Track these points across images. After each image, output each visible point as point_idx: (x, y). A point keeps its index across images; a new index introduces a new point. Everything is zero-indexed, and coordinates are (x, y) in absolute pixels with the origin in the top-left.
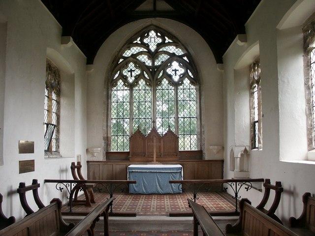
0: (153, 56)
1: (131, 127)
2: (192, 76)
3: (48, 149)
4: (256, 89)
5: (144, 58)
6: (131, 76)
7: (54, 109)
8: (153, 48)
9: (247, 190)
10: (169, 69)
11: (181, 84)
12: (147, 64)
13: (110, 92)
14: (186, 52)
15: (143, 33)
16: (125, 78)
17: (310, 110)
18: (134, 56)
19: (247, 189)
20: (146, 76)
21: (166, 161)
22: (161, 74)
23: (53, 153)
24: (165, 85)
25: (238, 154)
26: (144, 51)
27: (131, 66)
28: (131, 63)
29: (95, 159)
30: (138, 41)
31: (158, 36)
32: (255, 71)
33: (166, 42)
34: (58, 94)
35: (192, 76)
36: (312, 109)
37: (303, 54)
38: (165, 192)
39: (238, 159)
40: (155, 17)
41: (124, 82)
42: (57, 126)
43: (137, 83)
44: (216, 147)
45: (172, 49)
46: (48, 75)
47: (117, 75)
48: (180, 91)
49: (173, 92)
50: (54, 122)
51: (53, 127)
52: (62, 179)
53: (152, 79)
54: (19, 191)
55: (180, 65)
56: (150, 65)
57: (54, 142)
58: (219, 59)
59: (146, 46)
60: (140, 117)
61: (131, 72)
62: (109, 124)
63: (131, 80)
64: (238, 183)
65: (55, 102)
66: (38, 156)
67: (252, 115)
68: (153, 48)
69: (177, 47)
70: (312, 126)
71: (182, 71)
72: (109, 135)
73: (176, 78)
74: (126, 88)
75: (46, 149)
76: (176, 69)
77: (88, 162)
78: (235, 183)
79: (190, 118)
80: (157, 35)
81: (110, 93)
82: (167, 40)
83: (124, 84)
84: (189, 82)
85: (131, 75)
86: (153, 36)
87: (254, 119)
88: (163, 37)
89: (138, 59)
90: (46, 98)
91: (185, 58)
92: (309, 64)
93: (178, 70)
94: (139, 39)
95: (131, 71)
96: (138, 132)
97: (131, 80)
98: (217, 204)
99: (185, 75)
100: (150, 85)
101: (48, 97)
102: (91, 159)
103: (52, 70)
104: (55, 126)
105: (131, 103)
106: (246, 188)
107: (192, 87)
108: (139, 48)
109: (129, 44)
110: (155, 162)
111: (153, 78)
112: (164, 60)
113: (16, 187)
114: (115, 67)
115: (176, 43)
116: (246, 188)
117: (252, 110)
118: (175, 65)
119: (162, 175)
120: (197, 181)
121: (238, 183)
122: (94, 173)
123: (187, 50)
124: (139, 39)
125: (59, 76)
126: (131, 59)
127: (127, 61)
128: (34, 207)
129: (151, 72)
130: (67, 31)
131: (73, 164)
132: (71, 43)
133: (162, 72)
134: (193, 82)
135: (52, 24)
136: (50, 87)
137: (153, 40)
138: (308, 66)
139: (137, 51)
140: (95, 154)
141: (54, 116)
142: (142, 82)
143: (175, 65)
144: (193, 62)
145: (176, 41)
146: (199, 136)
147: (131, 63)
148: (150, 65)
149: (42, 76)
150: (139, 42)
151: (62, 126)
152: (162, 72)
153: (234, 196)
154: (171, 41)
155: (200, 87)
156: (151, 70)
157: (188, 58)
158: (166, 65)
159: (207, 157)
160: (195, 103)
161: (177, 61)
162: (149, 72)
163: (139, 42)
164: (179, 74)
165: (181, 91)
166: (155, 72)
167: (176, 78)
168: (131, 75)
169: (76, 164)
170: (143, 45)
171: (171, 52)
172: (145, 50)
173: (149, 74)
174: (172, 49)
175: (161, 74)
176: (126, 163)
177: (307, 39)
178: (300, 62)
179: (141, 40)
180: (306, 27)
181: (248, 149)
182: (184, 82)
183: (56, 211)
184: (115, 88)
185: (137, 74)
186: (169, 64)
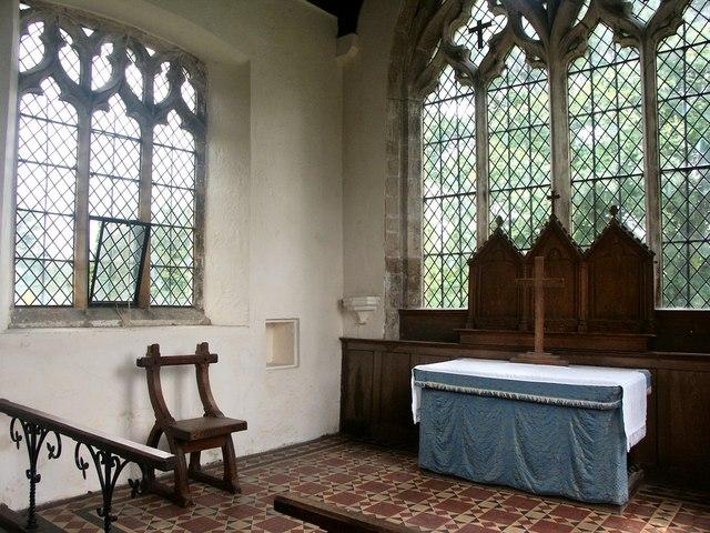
13: (412, 111)
16: (457, 56)
20: (530, 31)
21: (607, 352)
24: (602, 48)
29: (362, 333)
38: (545, 486)
49: (632, 72)
53: (545, 40)
62: (410, 218)
63: (477, 58)
74: (464, 90)
95: (480, 27)
99: (513, 34)
100: (542, 64)
110: (538, 353)
119: (540, 412)
122: (359, 377)
140: (364, 318)
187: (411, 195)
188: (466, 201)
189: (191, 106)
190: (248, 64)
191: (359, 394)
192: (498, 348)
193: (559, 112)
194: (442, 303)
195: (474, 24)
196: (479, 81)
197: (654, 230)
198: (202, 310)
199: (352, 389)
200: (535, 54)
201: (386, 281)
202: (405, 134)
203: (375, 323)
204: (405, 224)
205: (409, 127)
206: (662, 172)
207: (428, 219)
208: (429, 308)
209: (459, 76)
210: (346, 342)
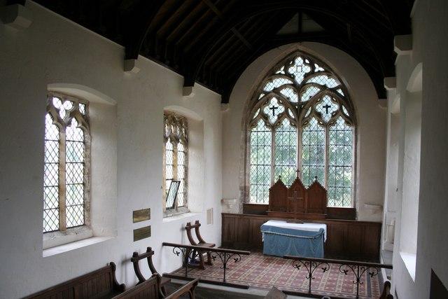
0: (300, 89)
2: (348, 114)
5: (289, 93)
8: (299, 79)
10: (319, 105)
14: (340, 84)
15: (288, 62)
16: (266, 118)
18: (276, 91)
21: (316, 219)
24: (314, 125)
27: (274, 101)
35: (348, 114)
44: (371, 206)
54: (132, 260)
59: (291, 77)
61: (274, 109)
68: (299, 79)
71: (335, 107)
72: (247, 185)
74: (267, 129)
76: (328, 106)
80: (304, 62)
82: (318, 68)
85: (274, 113)
91: (340, 91)
94: (282, 68)
95: (274, 108)
96: (280, 182)
97: (273, 120)
102: (226, 212)
109: (272, 75)
112: (313, 94)
113: (131, 255)
115: (328, 72)
118: (327, 100)
122: (229, 227)
123: (341, 81)
124: (282, 68)
126: (273, 94)
128: (147, 274)
133: (310, 108)
134: (350, 121)
137: (299, 69)
139: (281, 84)
140: (231, 206)
144: (349, 95)
150: (283, 73)
154: (322, 69)
158: (316, 99)
159: (360, 217)
161: (329, 95)
163: (283, 73)
164: (331, 112)
168: (274, 113)
171: (322, 84)
172: (290, 82)
179: (286, 70)
184: (255, 129)
185: (281, 112)
187: (248, 164)
190: (203, 121)
191: (229, 233)
192: (278, 217)
193: (300, 144)
195: (272, 107)
196: (327, 125)
197: (327, 185)
199: (226, 231)
200: (294, 123)
201: (239, 194)
202: (246, 142)
203: (235, 208)
204: (245, 174)
205: (247, 140)
209: (266, 125)
210: (223, 214)
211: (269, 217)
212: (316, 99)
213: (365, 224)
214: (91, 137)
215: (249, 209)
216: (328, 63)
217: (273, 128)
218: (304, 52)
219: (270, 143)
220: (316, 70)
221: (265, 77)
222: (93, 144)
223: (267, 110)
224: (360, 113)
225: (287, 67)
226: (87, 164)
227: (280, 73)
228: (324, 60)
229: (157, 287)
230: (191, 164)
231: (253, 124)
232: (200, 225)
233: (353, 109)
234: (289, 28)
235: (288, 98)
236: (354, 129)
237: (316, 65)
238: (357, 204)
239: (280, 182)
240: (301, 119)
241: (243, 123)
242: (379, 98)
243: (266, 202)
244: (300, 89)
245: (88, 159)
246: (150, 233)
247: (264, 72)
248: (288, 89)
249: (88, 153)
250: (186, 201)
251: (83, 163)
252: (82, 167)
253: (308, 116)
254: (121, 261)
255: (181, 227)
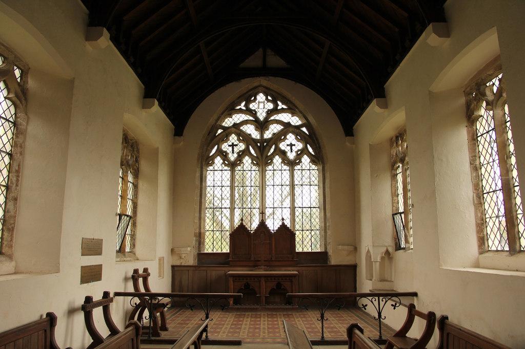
0: (261, 126)
1: (232, 220)
2: (313, 153)
3: (120, 249)
4: (400, 170)
5: (250, 130)
6: (233, 153)
7: (130, 195)
8: (262, 116)
9: (394, 308)
10: (283, 143)
11: (298, 164)
12: (254, 136)
13: (204, 173)
14: (305, 121)
15: (249, 97)
16: (224, 156)
17: (480, 198)
18: (236, 126)
19: (394, 306)
20: (253, 152)
22: (272, 150)
23: (126, 254)
25: (377, 256)
26: (250, 120)
27: (233, 138)
28: (233, 135)
30: (242, 106)
31: (268, 101)
32: (397, 145)
33: (279, 108)
34: (136, 175)
35: (313, 153)
36: (482, 197)
37: (466, 124)
39: (378, 264)
40: (264, 75)
41: (224, 160)
42: (133, 218)
43: (241, 161)
44: (346, 247)
45: (286, 117)
46: (124, 148)
47: (214, 151)
48: (297, 174)
49: (287, 174)
50: (129, 212)
51: (128, 218)
52: (126, 291)
53: (260, 157)
54: (83, 308)
55: (297, 138)
56: (258, 137)
57: (128, 238)
58: (349, 131)
59: (253, 113)
60: (245, 206)
61: (232, 146)
63: (232, 157)
64: (381, 298)
65: (131, 185)
66: (107, 260)
67: (395, 205)
68: (262, 116)
69: (293, 114)
70: (483, 220)
71: (299, 146)
72: (202, 231)
73: (291, 156)
74: (226, 168)
75: (118, 248)
76: (292, 144)
77: (173, 267)
78: (377, 298)
79: (311, 208)
80: (267, 99)
81: (204, 173)
82: (281, 106)
83: (224, 163)
84: (309, 160)
85: (233, 150)
86: (261, 100)
87: (398, 209)
88: (274, 102)
89: (241, 131)
90: (120, 180)
91: (304, 129)
92: (475, 137)
93: (294, 145)
94: (243, 104)
96: (242, 227)
97: (232, 157)
98: (332, 328)
99: (303, 151)
100: (257, 165)
101: (122, 178)
102: (178, 263)
103: (130, 143)
104: (131, 217)
105: (232, 188)
106: (392, 305)
107: (313, 167)
108: (243, 115)
109: (231, 110)
111: (262, 156)
112: (275, 131)
113: (81, 302)
114: (212, 139)
115: (292, 110)
116: (392, 305)
117: (395, 198)
118: (291, 138)
120: (326, 295)
121: (381, 298)
123: (306, 119)
124: (243, 104)
125: (138, 151)
126: (233, 129)
127: (227, 132)
128: (103, 330)
129: (259, 147)
130: (149, 93)
131: (136, 271)
132: (156, 108)
133: (274, 147)
134: (315, 160)
135: (131, 82)
136: (124, 164)
137: (261, 105)
138: (474, 139)
139: (241, 120)
140: (183, 256)
141: (130, 203)
142: (247, 160)
143: (291, 138)
144: (315, 135)
145: (291, 106)
146: (323, 233)
147: (233, 135)
148: (258, 137)
149: (117, 151)
150: (244, 108)
151: (140, 218)
152: (274, 147)
153: (377, 316)
154: (285, 107)
155: (323, 168)
156: (259, 144)
157: (308, 130)
158: (278, 138)
159: (334, 261)
160: (316, 188)
161: (293, 133)
162: (256, 147)
163: (244, 108)
164: (296, 150)
165: (299, 172)
166: (264, 147)
167: (291, 156)
168: (233, 150)
169: (141, 272)
170: (249, 111)
171: (286, 121)
172: (251, 118)
173: (257, 150)
174: (286, 117)
175: (272, 150)
176: (223, 269)
177: (471, 104)
178: (463, 134)
179: (247, 105)
180: (468, 89)
181: (390, 250)
182: (303, 160)
183: (133, 339)
184: (211, 168)
185: (241, 149)
186: (283, 137)
188: (314, 210)
189: (217, 146)
194: (213, 250)
195: (231, 144)
196: (292, 164)
198: (135, 254)
201: (194, 241)
203: (189, 258)
204: (200, 218)
205: (202, 179)
206: (295, 207)
207: (487, 210)
208: (207, 252)
211: (231, 266)
212: (278, 138)
213: (338, 267)
214: (28, 118)
215: (205, 259)
216: (293, 99)
217: (233, 165)
218: (267, 88)
219: (228, 183)
220: (279, 108)
221: (225, 111)
222: (30, 129)
223: (225, 147)
224: (329, 151)
225: (248, 102)
226: (15, 157)
227: (240, 108)
228: (289, 95)
229: (135, 341)
230: (141, 201)
231: (209, 161)
232: (149, 275)
233: (320, 147)
234: (254, 61)
235: (250, 135)
236: (321, 167)
237: (279, 103)
238: (328, 247)
239: (242, 227)
240: (264, 157)
241: (198, 160)
242: (346, 136)
243: (226, 249)
244: (261, 126)
245: (19, 149)
246: (101, 274)
247: (221, 108)
248: (249, 125)
249: (20, 140)
250: (133, 245)
251: (10, 155)
252: (7, 159)
253: (272, 154)
254: (67, 311)
255: (123, 276)
